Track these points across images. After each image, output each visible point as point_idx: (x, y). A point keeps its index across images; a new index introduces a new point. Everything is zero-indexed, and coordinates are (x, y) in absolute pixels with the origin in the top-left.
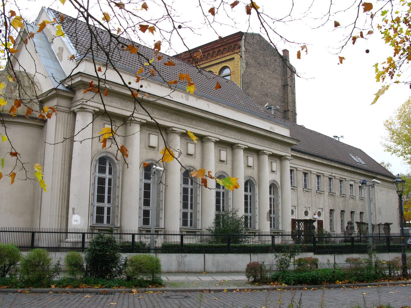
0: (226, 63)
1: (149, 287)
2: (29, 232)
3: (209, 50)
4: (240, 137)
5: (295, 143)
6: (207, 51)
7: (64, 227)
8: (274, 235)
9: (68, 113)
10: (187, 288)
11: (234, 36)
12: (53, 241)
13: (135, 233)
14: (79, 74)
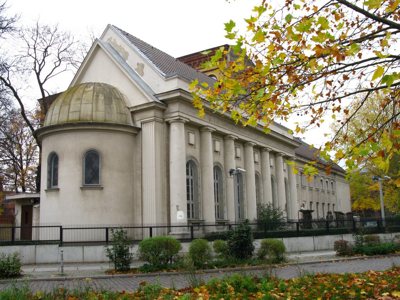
0: (212, 72)
1: (355, 256)
3: (195, 60)
4: (267, 141)
5: (298, 146)
6: (193, 60)
7: (166, 222)
8: (193, 226)
9: (162, 123)
10: (310, 261)
14: (179, 91)
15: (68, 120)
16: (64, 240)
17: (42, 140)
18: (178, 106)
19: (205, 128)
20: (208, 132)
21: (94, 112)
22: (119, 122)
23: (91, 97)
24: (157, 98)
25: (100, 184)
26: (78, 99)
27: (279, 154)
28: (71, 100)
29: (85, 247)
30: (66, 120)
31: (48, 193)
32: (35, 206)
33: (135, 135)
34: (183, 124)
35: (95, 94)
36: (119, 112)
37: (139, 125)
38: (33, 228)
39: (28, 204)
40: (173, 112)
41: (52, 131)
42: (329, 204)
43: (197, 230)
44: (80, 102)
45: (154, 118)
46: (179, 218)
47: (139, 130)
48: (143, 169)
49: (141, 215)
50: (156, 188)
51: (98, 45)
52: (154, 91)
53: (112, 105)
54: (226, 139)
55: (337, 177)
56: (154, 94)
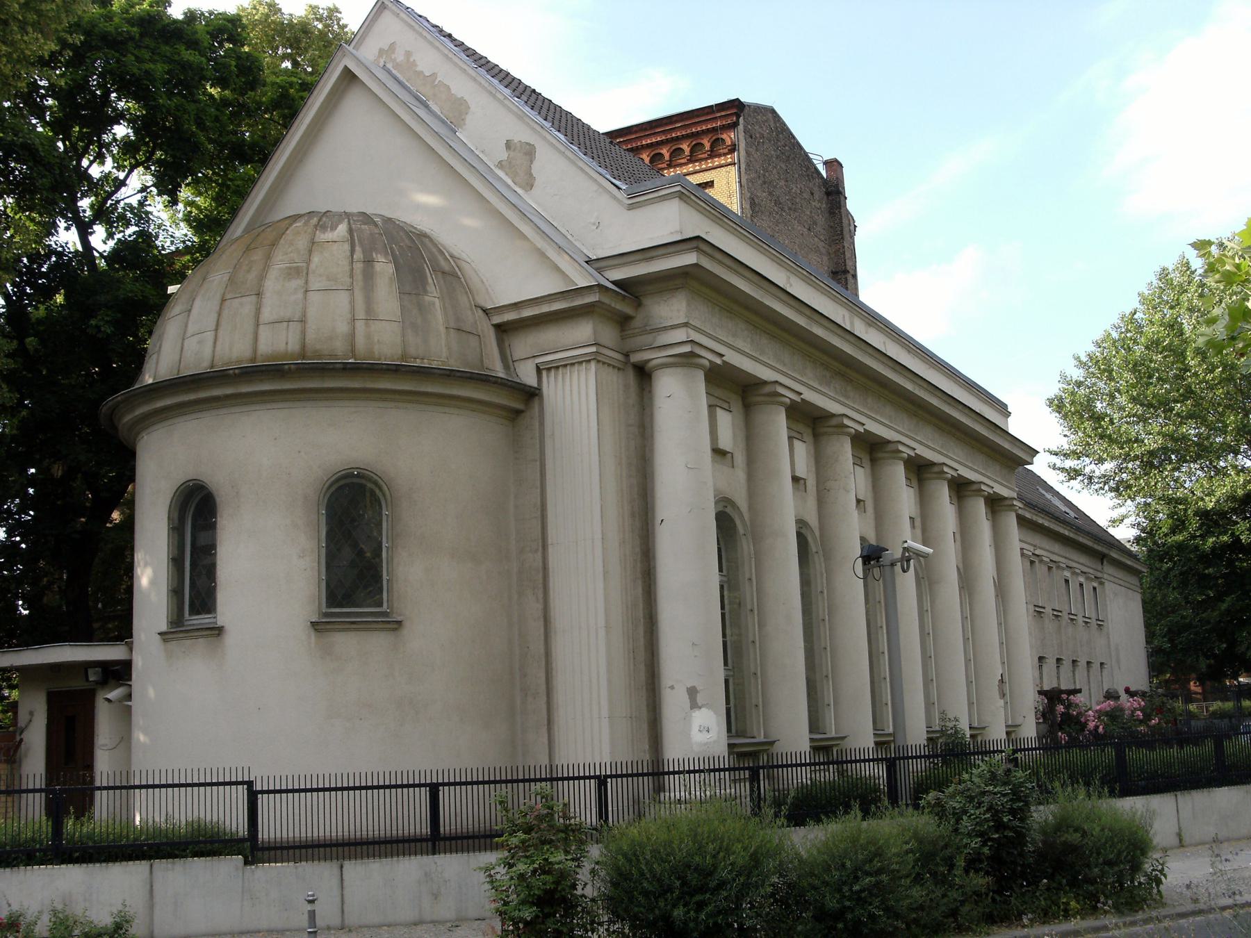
2: (420, 785)
9: (619, 369)
11: (713, 112)
12: (626, 804)
13: (440, 781)
14: (694, 244)
15: (255, 350)
16: (445, 827)
17: (138, 433)
18: (684, 304)
19: (768, 389)
20: (774, 406)
21: (360, 326)
22: (454, 365)
23: (345, 263)
24: (599, 271)
25: (385, 605)
26: (294, 272)
27: (975, 487)
28: (262, 277)
29: (348, 865)
30: (248, 353)
31: (173, 645)
32: (109, 696)
33: (515, 415)
34: (702, 373)
35: (358, 254)
36: (452, 324)
37: (527, 375)
38: (98, 793)
39: (77, 684)
40: (665, 329)
41: (192, 397)
42: (1089, 663)
43: (740, 780)
44: (300, 282)
45: (593, 349)
46: (698, 737)
47: (531, 395)
48: (550, 550)
49: (545, 729)
50: (607, 621)
51: (347, 72)
52: (585, 251)
53: (426, 298)
54: (826, 433)
55: (1109, 569)
56: (587, 260)
